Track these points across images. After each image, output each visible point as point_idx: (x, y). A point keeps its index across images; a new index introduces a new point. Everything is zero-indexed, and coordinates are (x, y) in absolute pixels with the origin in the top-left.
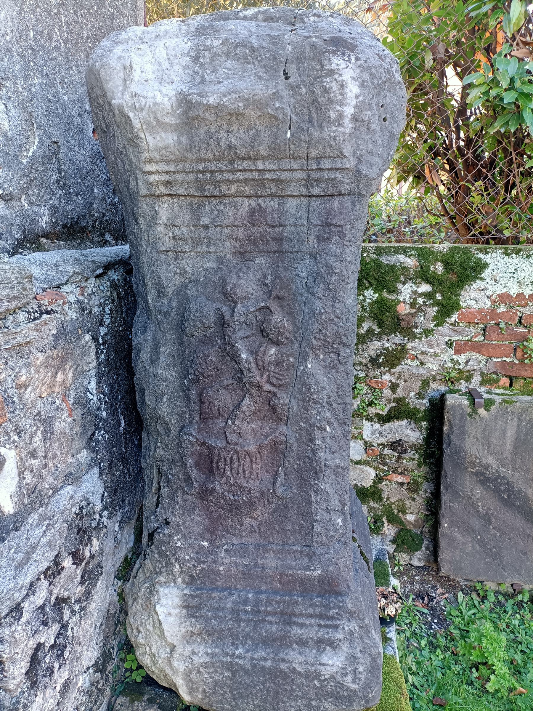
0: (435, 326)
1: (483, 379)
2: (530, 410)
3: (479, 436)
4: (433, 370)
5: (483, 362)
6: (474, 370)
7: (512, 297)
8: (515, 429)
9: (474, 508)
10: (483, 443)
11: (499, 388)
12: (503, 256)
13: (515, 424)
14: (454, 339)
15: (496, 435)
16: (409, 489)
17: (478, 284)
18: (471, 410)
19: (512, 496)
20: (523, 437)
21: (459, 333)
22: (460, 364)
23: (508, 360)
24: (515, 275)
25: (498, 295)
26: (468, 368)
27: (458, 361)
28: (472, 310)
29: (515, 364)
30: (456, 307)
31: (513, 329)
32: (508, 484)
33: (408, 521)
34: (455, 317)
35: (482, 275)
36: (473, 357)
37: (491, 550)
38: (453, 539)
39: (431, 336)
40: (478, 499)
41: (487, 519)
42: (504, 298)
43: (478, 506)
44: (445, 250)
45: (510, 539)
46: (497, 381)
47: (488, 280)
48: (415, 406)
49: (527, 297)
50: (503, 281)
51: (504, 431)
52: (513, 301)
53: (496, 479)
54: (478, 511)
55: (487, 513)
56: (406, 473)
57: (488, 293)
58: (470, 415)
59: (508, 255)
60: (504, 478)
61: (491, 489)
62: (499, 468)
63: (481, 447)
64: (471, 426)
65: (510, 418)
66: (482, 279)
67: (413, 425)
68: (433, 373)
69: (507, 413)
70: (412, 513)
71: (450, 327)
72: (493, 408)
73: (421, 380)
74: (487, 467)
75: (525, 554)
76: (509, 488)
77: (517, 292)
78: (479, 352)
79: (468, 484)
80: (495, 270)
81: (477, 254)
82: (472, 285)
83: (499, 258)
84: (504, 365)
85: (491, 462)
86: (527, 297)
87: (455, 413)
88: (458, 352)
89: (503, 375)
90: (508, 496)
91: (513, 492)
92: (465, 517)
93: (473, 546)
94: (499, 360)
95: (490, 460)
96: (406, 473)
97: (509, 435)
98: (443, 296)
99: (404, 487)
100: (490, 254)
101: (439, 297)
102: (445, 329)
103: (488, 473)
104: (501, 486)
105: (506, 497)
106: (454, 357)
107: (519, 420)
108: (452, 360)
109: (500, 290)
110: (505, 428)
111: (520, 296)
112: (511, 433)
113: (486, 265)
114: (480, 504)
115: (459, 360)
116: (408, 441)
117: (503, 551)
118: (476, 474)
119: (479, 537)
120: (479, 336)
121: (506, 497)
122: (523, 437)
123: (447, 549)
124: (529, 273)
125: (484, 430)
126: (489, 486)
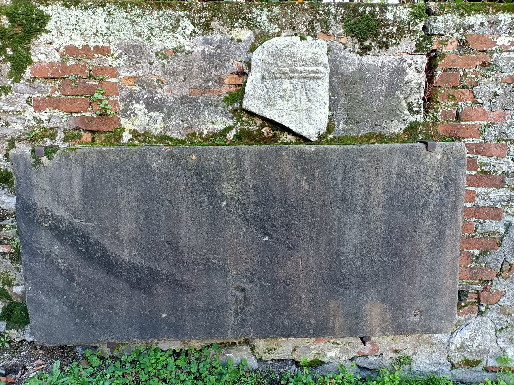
0: (13, 83)
1: (65, 136)
2: (91, 155)
3: (47, 187)
4: (17, 130)
5: (65, 119)
6: (58, 127)
7: (78, 49)
8: (80, 177)
9: (55, 265)
10: (51, 195)
11: (82, 144)
12: (63, 8)
13: (79, 171)
14: (33, 96)
15: (63, 184)
16: (11, 259)
17: (44, 37)
18: (34, 160)
19: (90, 248)
20: (89, 185)
21: (38, 89)
22: (43, 122)
23: (87, 115)
24: (77, 27)
25: (65, 48)
26: (52, 125)
27: (40, 119)
28: (43, 64)
29: (93, 118)
30: (28, 61)
31: (85, 82)
32: (83, 236)
33: (15, 294)
34: (28, 73)
35: (47, 28)
36: (55, 114)
37: (79, 310)
38: (39, 303)
39: (9, 94)
40: (57, 255)
41: (70, 276)
42: (71, 50)
43: (59, 263)
44: (8, 3)
45: (95, 295)
46: (79, 137)
47: (53, 33)
48: (6, 169)
49: (92, 49)
50: (67, 33)
51: (70, 180)
52: (80, 54)
53: (71, 232)
54: (60, 269)
55: (69, 270)
56: (6, 242)
57: (56, 46)
58: (34, 166)
59: (68, 7)
60: (78, 230)
61: (68, 242)
62: (72, 219)
63: (50, 199)
64: (37, 177)
65: (73, 165)
66: (47, 32)
67: (6, 190)
68: (18, 132)
69: (70, 160)
70: (18, 285)
71: (27, 83)
72: (55, 156)
73: (7, 141)
74: (60, 220)
75: (113, 309)
76: (85, 240)
77: (82, 44)
78: (56, 108)
79: (45, 240)
80: (58, 22)
81: (39, 6)
82: (39, 38)
83: (60, 10)
84: (84, 120)
85: (63, 214)
86: (92, 49)
87: (18, 164)
88: (38, 109)
89: (85, 131)
90: (85, 249)
91: (90, 244)
92: (48, 277)
93: (60, 308)
94: (79, 115)
95: (62, 212)
96: (6, 242)
97: (75, 183)
98: (13, 50)
99: (7, 258)
100: (50, 6)
101: (9, 51)
102: (21, 85)
103: (61, 226)
104: (77, 238)
105: (83, 250)
106: (36, 114)
107: (83, 166)
108: (35, 118)
109: (64, 42)
110: (71, 176)
111: (85, 48)
112: (77, 180)
113: (48, 18)
114: (60, 261)
115: (41, 117)
116: (7, 208)
117: (90, 308)
118: (50, 228)
119: (65, 297)
120: (56, 92)
121: (83, 250)
122: (89, 185)
123: (34, 314)
124: (89, 24)
125: (50, 181)
126: (66, 240)
